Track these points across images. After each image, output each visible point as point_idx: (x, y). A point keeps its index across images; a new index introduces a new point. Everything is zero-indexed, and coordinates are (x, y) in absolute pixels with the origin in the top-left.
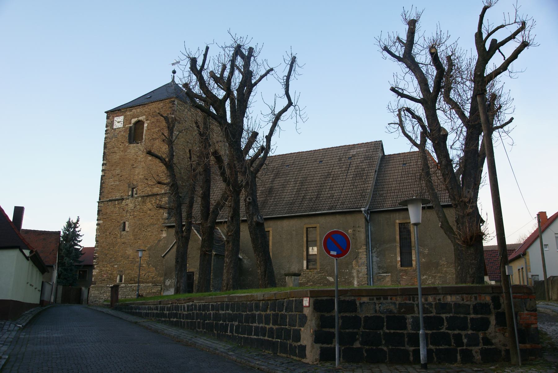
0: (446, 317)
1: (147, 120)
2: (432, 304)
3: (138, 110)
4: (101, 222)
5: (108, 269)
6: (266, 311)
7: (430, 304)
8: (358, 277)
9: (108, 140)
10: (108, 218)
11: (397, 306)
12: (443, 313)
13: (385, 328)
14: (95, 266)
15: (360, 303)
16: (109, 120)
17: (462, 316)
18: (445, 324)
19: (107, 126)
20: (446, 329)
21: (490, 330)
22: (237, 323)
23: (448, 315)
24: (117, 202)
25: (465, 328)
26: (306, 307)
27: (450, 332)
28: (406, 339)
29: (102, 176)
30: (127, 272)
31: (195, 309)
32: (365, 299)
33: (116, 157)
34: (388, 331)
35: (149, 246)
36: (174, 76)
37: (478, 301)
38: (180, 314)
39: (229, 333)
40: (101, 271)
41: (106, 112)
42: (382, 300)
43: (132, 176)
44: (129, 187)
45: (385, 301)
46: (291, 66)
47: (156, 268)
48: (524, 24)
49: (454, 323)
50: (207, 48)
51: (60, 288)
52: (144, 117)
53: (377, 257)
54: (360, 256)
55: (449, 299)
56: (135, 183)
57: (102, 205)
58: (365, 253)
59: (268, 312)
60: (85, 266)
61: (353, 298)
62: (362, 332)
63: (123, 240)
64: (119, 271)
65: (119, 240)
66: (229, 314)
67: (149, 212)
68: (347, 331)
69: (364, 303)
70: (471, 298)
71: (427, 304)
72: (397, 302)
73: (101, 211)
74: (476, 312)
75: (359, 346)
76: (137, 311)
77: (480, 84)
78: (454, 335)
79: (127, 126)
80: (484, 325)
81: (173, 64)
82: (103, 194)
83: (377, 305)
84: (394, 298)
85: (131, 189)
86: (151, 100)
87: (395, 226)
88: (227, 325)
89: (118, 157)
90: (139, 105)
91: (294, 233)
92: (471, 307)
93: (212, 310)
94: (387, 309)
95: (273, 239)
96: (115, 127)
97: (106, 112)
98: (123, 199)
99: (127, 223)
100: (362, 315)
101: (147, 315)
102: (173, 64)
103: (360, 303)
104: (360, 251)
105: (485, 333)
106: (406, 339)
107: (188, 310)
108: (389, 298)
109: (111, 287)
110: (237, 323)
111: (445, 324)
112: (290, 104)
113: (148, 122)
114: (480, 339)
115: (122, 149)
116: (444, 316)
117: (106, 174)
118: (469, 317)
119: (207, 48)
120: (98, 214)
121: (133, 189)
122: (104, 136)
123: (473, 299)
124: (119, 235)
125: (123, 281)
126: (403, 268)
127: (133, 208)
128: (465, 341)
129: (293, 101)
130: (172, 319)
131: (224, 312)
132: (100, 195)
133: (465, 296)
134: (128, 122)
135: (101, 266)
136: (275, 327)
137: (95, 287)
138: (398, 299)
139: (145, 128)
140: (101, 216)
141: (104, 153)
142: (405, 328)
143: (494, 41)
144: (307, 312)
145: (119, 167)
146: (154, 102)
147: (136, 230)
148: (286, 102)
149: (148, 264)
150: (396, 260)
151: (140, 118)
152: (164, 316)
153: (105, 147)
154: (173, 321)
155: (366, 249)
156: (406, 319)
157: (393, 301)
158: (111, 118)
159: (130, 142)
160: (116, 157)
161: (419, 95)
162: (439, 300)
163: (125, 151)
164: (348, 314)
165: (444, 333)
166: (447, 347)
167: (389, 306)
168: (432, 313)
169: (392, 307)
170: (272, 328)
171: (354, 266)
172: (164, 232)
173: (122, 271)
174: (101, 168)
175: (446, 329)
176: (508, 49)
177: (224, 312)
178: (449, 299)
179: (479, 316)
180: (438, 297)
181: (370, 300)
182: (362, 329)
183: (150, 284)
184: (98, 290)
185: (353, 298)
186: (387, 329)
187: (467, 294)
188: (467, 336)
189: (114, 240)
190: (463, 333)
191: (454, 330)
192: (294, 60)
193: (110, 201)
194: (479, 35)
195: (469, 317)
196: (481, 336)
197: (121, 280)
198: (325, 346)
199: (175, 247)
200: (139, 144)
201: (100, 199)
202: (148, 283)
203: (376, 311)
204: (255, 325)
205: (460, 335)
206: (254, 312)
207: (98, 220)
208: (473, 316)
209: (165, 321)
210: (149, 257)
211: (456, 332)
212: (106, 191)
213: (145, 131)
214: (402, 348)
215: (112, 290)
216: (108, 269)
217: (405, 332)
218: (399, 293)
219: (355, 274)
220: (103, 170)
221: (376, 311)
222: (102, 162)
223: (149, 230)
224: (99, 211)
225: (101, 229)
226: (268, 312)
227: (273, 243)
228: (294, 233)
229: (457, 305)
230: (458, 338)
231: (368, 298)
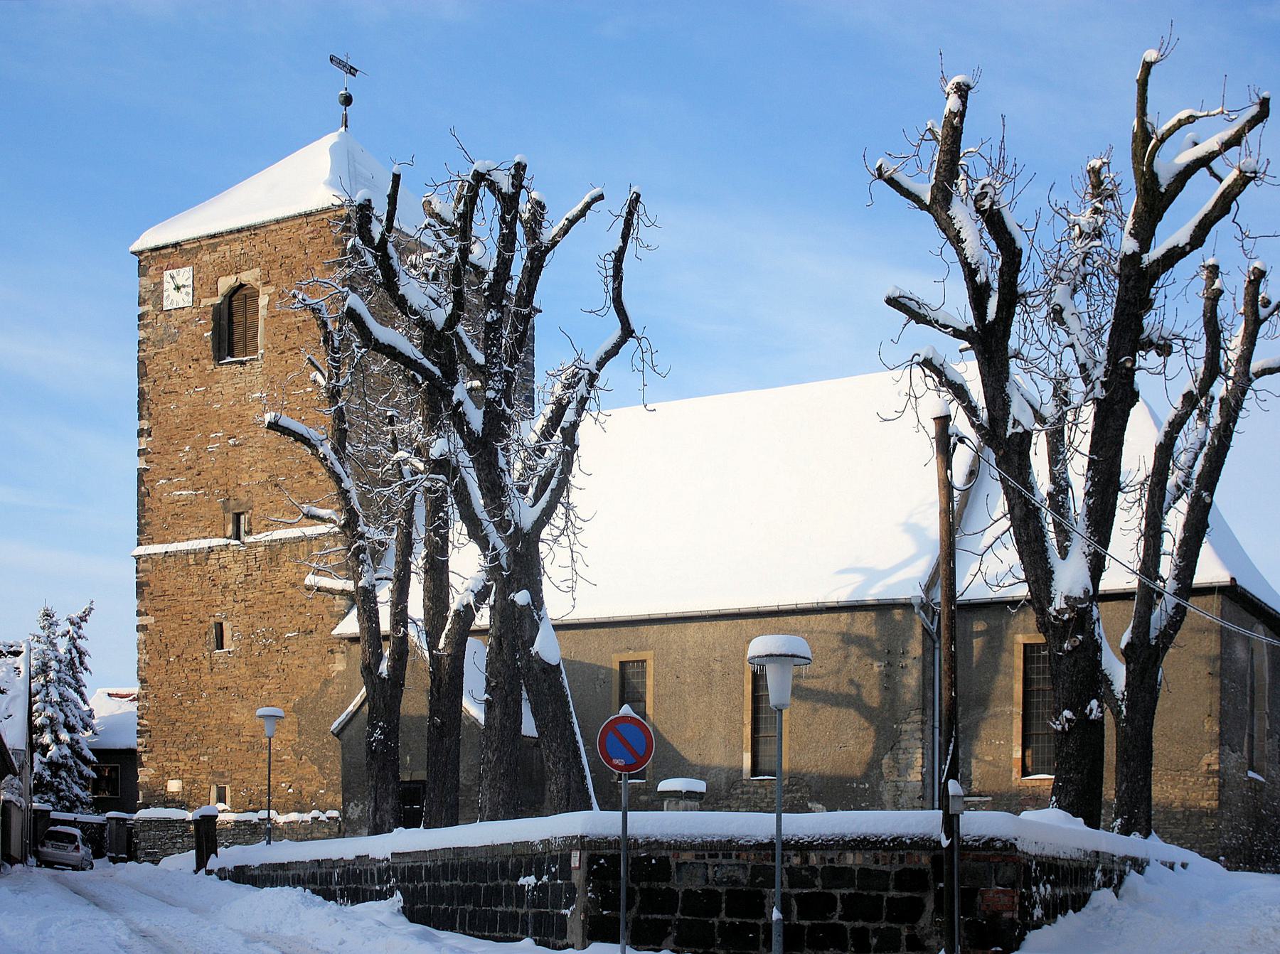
0: (842, 896)
3: (237, 247)
4: (149, 620)
5: (181, 765)
7: (813, 869)
9: (151, 351)
12: (837, 887)
13: (723, 914)
14: (144, 758)
16: (146, 281)
17: (873, 893)
18: (839, 909)
20: (840, 918)
21: (921, 923)
23: (846, 892)
25: (875, 917)
26: (576, 868)
27: (844, 923)
30: (239, 776)
37: (906, 865)
42: (720, 860)
43: (232, 474)
44: (226, 510)
45: (724, 862)
46: (628, 225)
47: (320, 768)
48: (1265, 103)
49: (853, 907)
50: (396, 178)
54: (903, 745)
56: (243, 498)
58: (919, 735)
62: (679, 920)
63: (218, 679)
65: (207, 678)
66: (458, 887)
67: (289, 591)
69: (685, 863)
71: (806, 870)
74: (898, 887)
77: (1131, 283)
78: (854, 930)
79: (204, 302)
80: (912, 911)
82: (148, 530)
85: (230, 516)
88: (454, 912)
91: (718, 667)
94: (729, 878)
95: (657, 685)
96: (167, 305)
103: (677, 864)
104: (904, 727)
112: (627, 332)
113: (272, 289)
114: (903, 938)
116: (837, 892)
118: (886, 895)
119: (396, 178)
121: (238, 516)
124: (206, 663)
129: (634, 326)
139: (262, 312)
140: (147, 602)
144: (577, 878)
145: (191, 441)
148: (617, 332)
150: (1011, 757)
155: (923, 722)
156: (765, 897)
157: (741, 862)
158: (152, 271)
159: (218, 357)
161: (964, 316)
162: (832, 860)
167: (729, 868)
168: (815, 886)
169: (739, 874)
171: (885, 770)
172: (339, 656)
173: (222, 775)
175: (840, 918)
176: (1200, 196)
178: (851, 859)
179: (906, 894)
181: (697, 857)
182: (678, 915)
188: (877, 932)
189: (194, 677)
190: (871, 926)
192: (636, 199)
194: (1143, 135)
195: (886, 895)
196: (905, 933)
203: (707, 880)
204: (500, 909)
207: (139, 613)
208: (892, 893)
210: (300, 733)
211: (860, 924)
212: (158, 522)
216: (181, 765)
221: (707, 880)
225: (154, 645)
227: (656, 696)
228: (718, 667)
229: (865, 872)
231: (693, 853)
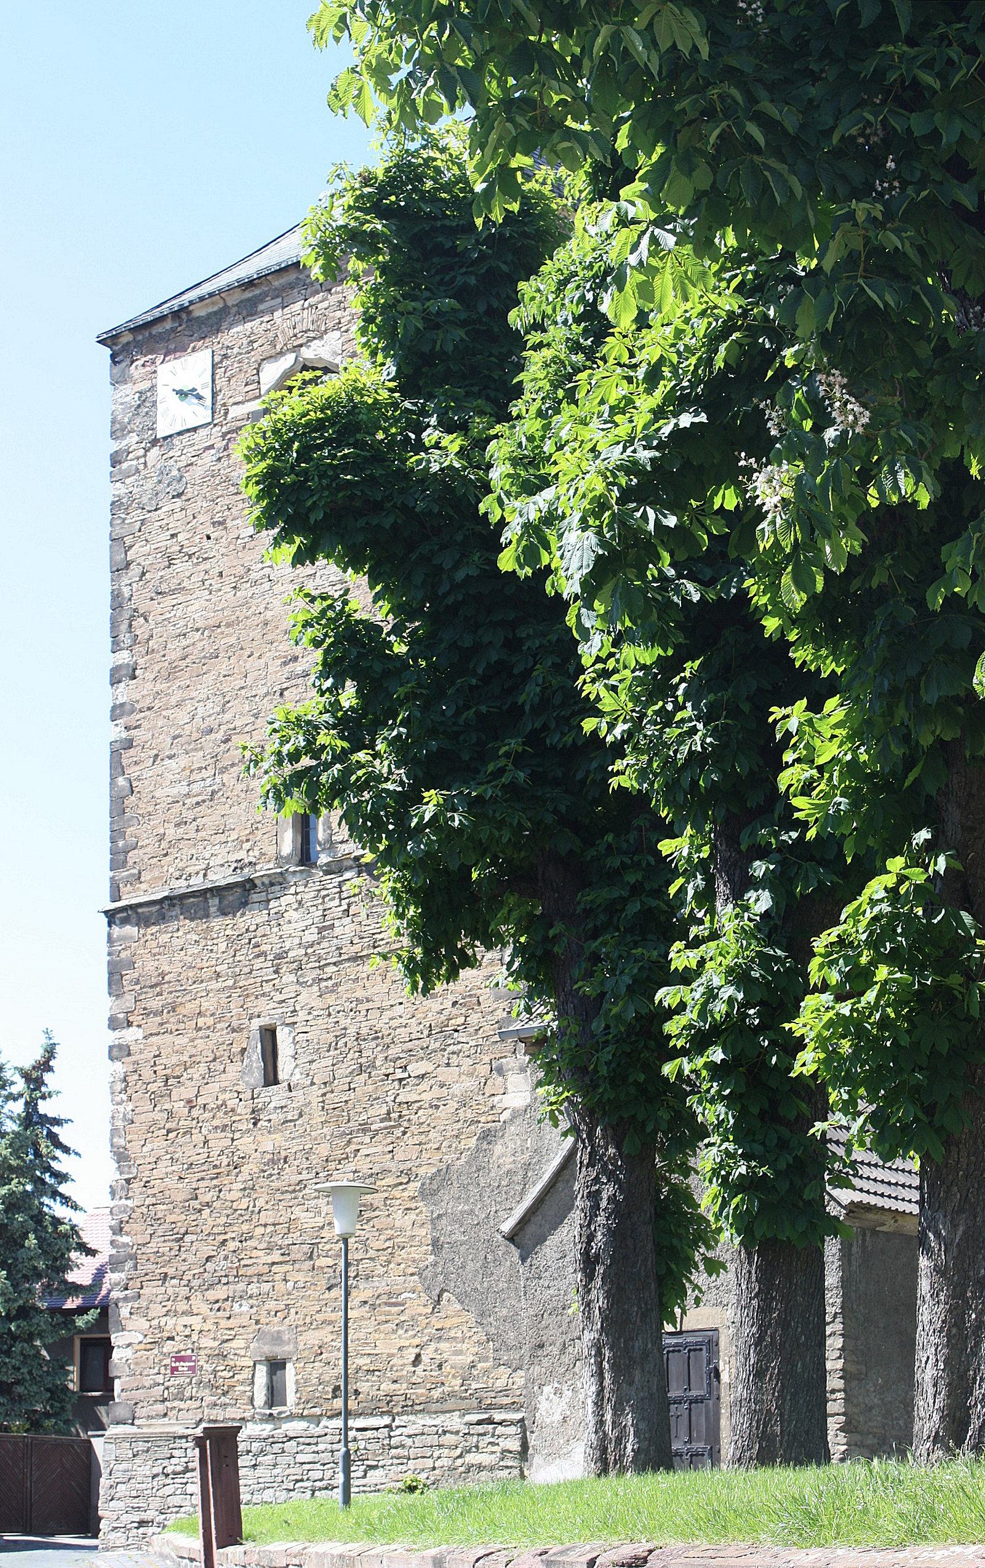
5: (195, 1322)
19: (118, 431)
29: (120, 750)
125: (291, 1397)
201: (116, 896)
216: (195, 1322)
220: (117, 712)
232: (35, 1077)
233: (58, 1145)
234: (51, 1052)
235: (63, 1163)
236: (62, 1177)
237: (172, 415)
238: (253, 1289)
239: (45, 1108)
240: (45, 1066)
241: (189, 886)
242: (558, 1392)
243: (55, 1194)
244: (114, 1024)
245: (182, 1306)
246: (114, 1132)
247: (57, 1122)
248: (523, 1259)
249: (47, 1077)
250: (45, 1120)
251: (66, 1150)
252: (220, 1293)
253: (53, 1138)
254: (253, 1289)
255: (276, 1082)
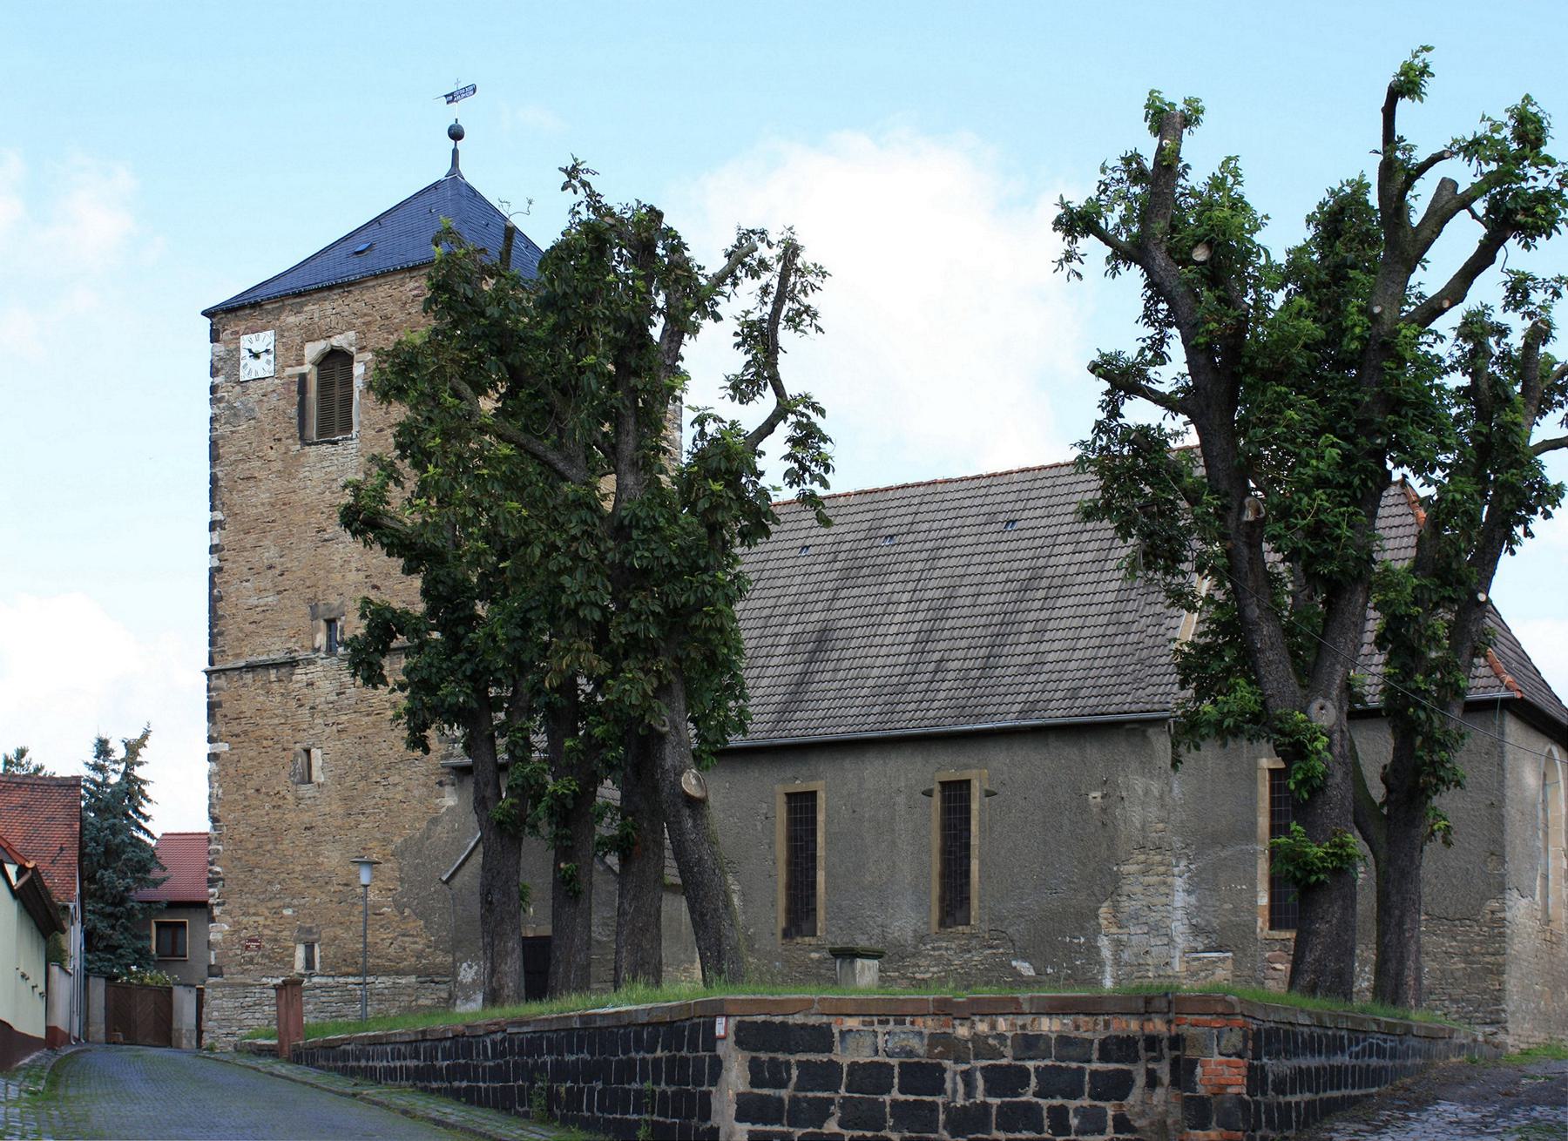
0: (1037, 1069)
1: (362, 349)
2: (1006, 1038)
4: (223, 747)
5: (261, 920)
6: (654, 1051)
7: (1001, 1037)
8: (1117, 962)
10: (245, 733)
11: (926, 1041)
14: (216, 911)
15: (841, 1032)
17: (1074, 1065)
19: (214, 372)
21: (1131, 1099)
22: (599, 1085)
23: (1042, 1064)
24: (273, 674)
25: (1075, 1094)
28: (942, 1117)
29: (214, 572)
30: (327, 933)
31: (512, 1053)
32: (852, 1023)
33: (258, 498)
34: (902, 1097)
35: (398, 840)
36: (455, 153)
37: (1112, 1032)
38: (476, 1067)
39: (586, 1114)
40: (237, 928)
41: (205, 313)
44: (314, 617)
45: (898, 1029)
49: (1053, 1082)
51: (98, 987)
52: (351, 334)
53: (1189, 893)
55: (1047, 1025)
56: (335, 600)
57: (222, 682)
59: (659, 1053)
60: (175, 905)
61: (825, 1019)
63: (306, 818)
64: (300, 928)
66: (585, 1062)
68: (810, 1094)
70: (1096, 1024)
72: (926, 1031)
73: (219, 704)
74: (1104, 1057)
75: (836, 1129)
76: (363, 1063)
78: (1051, 1108)
79: (289, 371)
81: (451, 98)
83: (880, 1036)
84: (919, 1020)
85: (322, 624)
86: (373, 262)
87: (1254, 781)
88: (581, 1091)
89: (264, 497)
90: (330, 288)
92: (1096, 1045)
93: (550, 1053)
97: (205, 313)
98: (293, 664)
99: (316, 753)
100: (844, 1056)
101: (391, 1074)
102: (451, 98)
103: (841, 1032)
104: (1125, 869)
105: (1121, 1106)
106: (942, 1117)
107: (494, 1057)
108: (908, 1019)
109: (275, 987)
110: (599, 1085)
111: (1033, 1081)
115: (278, 466)
116: (1030, 1064)
117: (227, 566)
120: (211, 716)
122: (207, 412)
123: (1100, 1027)
125: (317, 966)
126: (1277, 934)
127: (333, 697)
128: (1074, 1122)
130: (456, 1084)
131: (574, 1058)
132: (212, 643)
133: (1082, 1019)
134: (293, 354)
135: (237, 912)
136: (670, 1090)
137: (224, 985)
138: (930, 1023)
141: (214, 480)
142: (940, 1090)
143: (1447, 185)
146: (384, 274)
147: (349, 782)
149: (399, 907)
151: (338, 341)
152: (435, 1074)
153: (214, 457)
154: (459, 1089)
157: (916, 1028)
160: (258, 498)
162: (1023, 1027)
163: (287, 473)
164: (812, 1057)
165: (1028, 1103)
166: (1033, 1135)
169: (914, 1043)
170: (664, 1093)
171: (1103, 922)
173: (309, 931)
174: (205, 539)
177: (574, 1058)
178: (1047, 1025)
180: (1020, 1021)
183: (413, 979)
184: (233, 996)
185: (825, 1019)
186: (901, 1091)
187: (1087, 1014)
189: (277, 814)
190: (1072, 1104)
191: (1053, 1097)
193: (251, 668)
197: (309, 963)
198: (759, 1127)
199: (478, 859)
200: (340, 448)
201: (211, 662)
202: (400, 973)
203: (876, 1052)
204: (635, 1086)
205: (1063, 1110)
206: (633, 1054)
209: (439, 1090)
211: (1058, 1102)
213: (356, 395)
214: (932, 1136)
215: (279, 997)
216: (261, 920)
217: (939, 1100)
218: (931, 1010)
219: (1106, 953)
220: (214, 549)
222: (206, 516)
223: (396, 779)
224: (212, 707)
226: (659, 1053)
229: (1064, 1041)
230: (1059, 1115)
232: (133, 748)
233: (145, 797)
234: (145, 737)
235: (146, 809)
236: (147, 818)
237: (252, 369)
238: (295, 902)
239: (138, 772)
240: (141, 742)
241: (363, 1020)
242: (470, 967)
243: (140, 827)
244: (211, 740)
245: (252, 910)
246: (211, 806)
247: (144, 782)
248: (787, 934)
249: (141, 751)
250: (137, 779)
251: (149, 801)
252: (277, 904)
253: (142, 792)
254: (295, 902)
255: (310, 781)
